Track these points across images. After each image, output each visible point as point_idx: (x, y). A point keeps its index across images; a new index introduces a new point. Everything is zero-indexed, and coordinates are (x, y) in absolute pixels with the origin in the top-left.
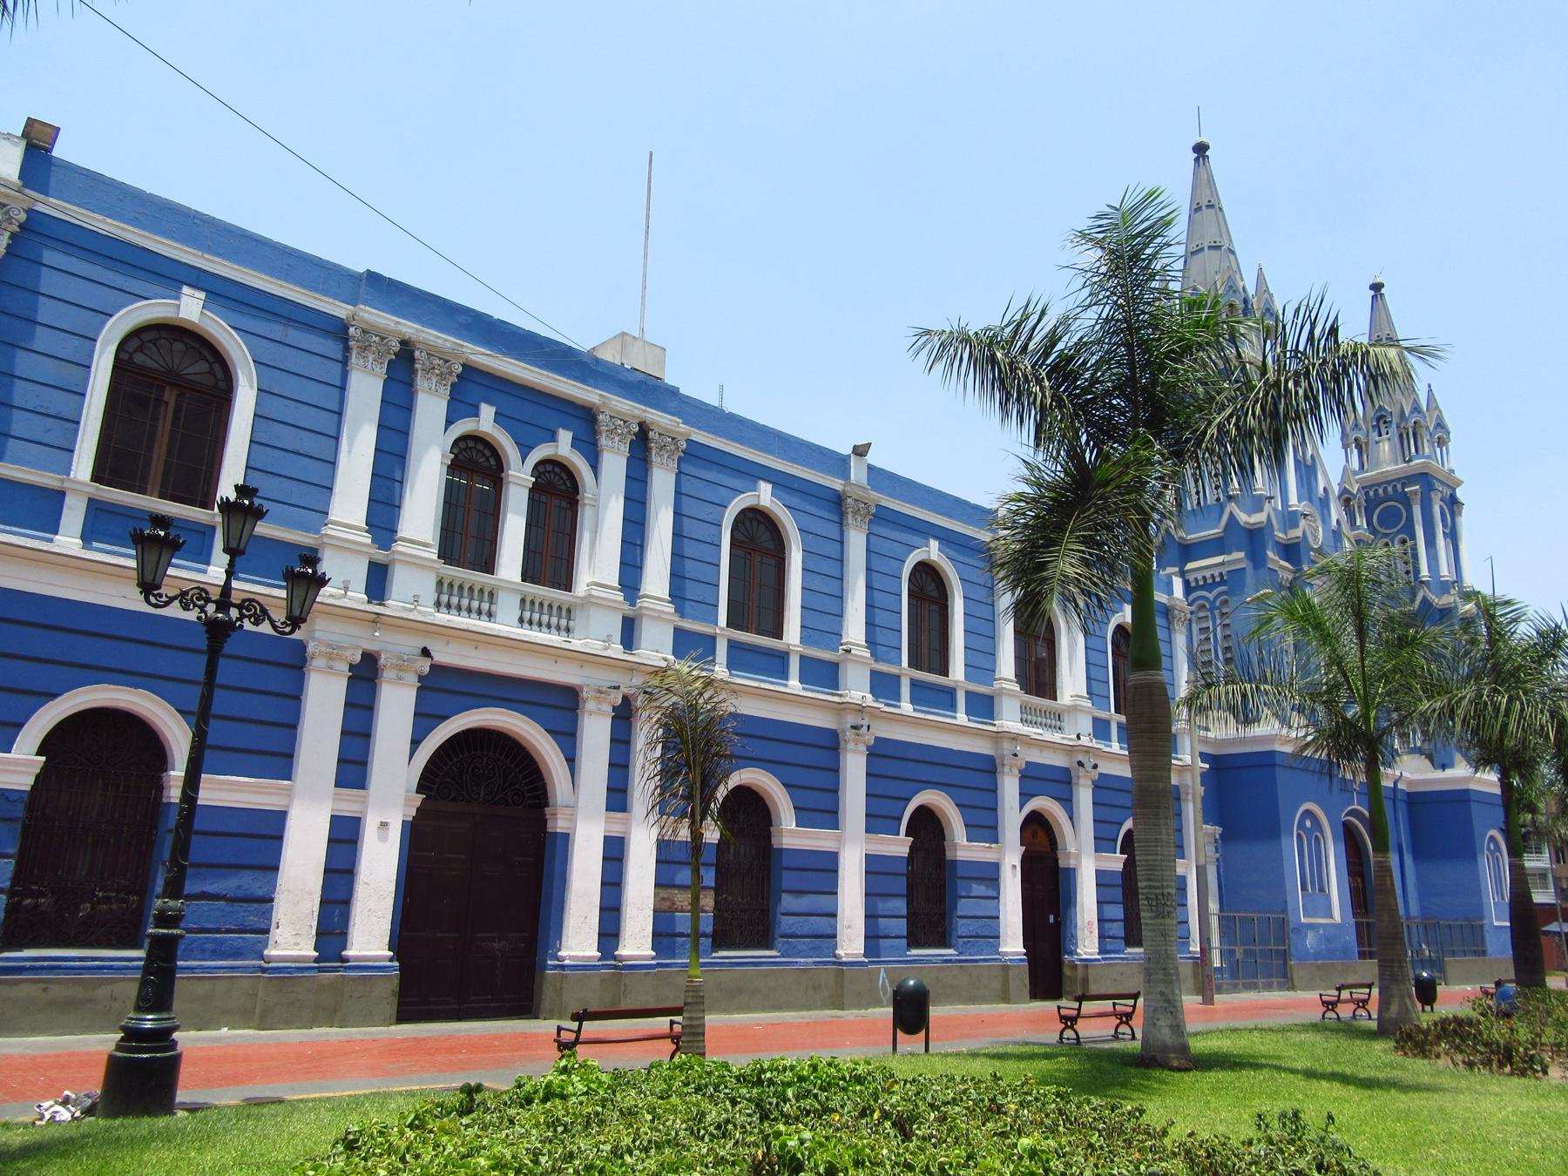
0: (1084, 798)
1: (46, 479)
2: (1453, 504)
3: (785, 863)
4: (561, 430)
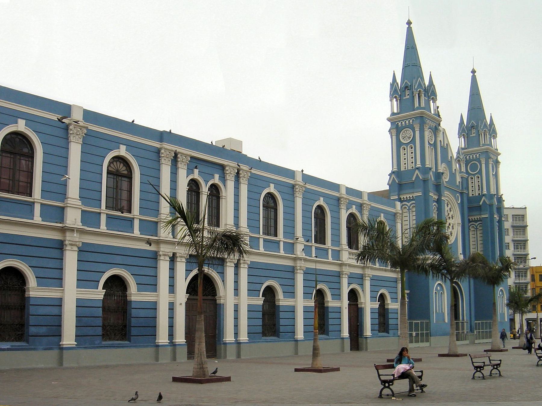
0: (367, 284)
1: (97, 210)
2: (497, 163)
3: (390, 312)
4: (216, 174)
